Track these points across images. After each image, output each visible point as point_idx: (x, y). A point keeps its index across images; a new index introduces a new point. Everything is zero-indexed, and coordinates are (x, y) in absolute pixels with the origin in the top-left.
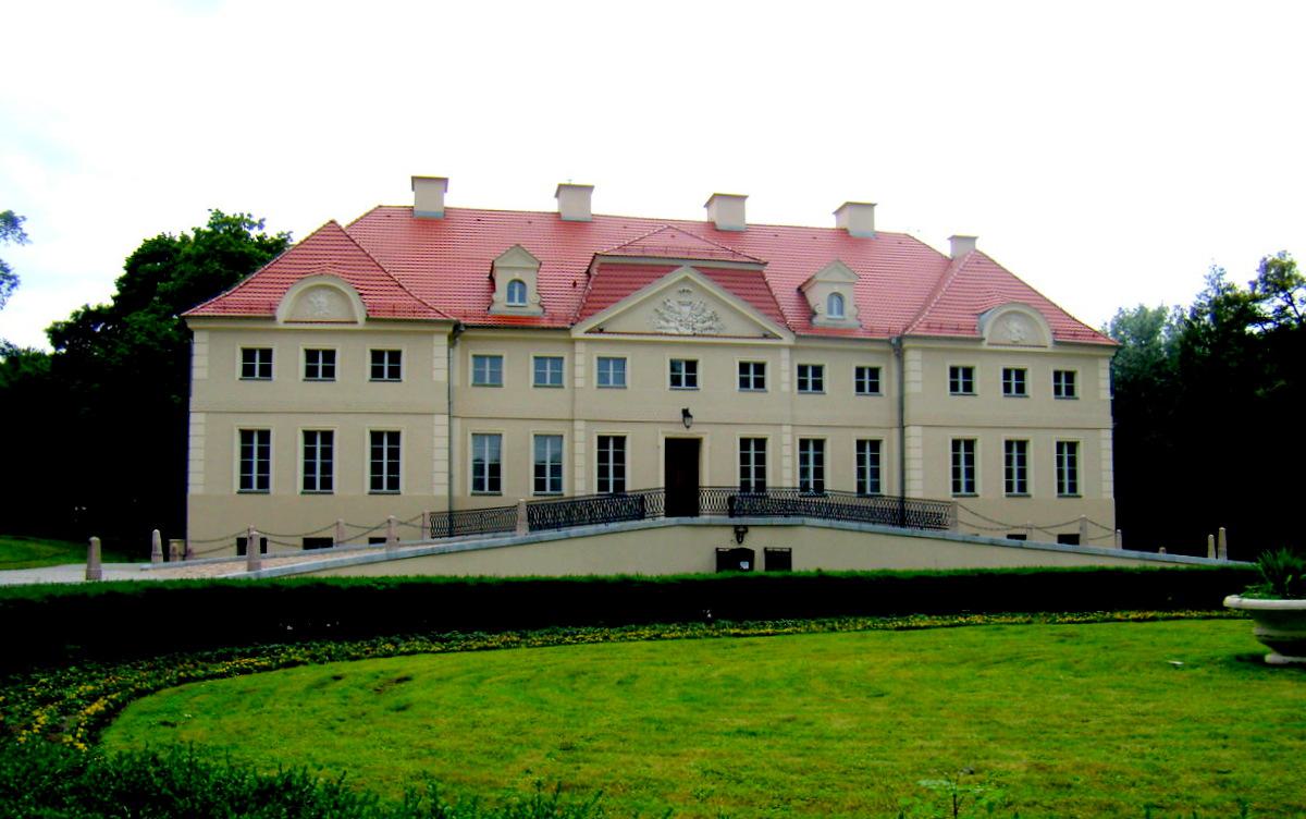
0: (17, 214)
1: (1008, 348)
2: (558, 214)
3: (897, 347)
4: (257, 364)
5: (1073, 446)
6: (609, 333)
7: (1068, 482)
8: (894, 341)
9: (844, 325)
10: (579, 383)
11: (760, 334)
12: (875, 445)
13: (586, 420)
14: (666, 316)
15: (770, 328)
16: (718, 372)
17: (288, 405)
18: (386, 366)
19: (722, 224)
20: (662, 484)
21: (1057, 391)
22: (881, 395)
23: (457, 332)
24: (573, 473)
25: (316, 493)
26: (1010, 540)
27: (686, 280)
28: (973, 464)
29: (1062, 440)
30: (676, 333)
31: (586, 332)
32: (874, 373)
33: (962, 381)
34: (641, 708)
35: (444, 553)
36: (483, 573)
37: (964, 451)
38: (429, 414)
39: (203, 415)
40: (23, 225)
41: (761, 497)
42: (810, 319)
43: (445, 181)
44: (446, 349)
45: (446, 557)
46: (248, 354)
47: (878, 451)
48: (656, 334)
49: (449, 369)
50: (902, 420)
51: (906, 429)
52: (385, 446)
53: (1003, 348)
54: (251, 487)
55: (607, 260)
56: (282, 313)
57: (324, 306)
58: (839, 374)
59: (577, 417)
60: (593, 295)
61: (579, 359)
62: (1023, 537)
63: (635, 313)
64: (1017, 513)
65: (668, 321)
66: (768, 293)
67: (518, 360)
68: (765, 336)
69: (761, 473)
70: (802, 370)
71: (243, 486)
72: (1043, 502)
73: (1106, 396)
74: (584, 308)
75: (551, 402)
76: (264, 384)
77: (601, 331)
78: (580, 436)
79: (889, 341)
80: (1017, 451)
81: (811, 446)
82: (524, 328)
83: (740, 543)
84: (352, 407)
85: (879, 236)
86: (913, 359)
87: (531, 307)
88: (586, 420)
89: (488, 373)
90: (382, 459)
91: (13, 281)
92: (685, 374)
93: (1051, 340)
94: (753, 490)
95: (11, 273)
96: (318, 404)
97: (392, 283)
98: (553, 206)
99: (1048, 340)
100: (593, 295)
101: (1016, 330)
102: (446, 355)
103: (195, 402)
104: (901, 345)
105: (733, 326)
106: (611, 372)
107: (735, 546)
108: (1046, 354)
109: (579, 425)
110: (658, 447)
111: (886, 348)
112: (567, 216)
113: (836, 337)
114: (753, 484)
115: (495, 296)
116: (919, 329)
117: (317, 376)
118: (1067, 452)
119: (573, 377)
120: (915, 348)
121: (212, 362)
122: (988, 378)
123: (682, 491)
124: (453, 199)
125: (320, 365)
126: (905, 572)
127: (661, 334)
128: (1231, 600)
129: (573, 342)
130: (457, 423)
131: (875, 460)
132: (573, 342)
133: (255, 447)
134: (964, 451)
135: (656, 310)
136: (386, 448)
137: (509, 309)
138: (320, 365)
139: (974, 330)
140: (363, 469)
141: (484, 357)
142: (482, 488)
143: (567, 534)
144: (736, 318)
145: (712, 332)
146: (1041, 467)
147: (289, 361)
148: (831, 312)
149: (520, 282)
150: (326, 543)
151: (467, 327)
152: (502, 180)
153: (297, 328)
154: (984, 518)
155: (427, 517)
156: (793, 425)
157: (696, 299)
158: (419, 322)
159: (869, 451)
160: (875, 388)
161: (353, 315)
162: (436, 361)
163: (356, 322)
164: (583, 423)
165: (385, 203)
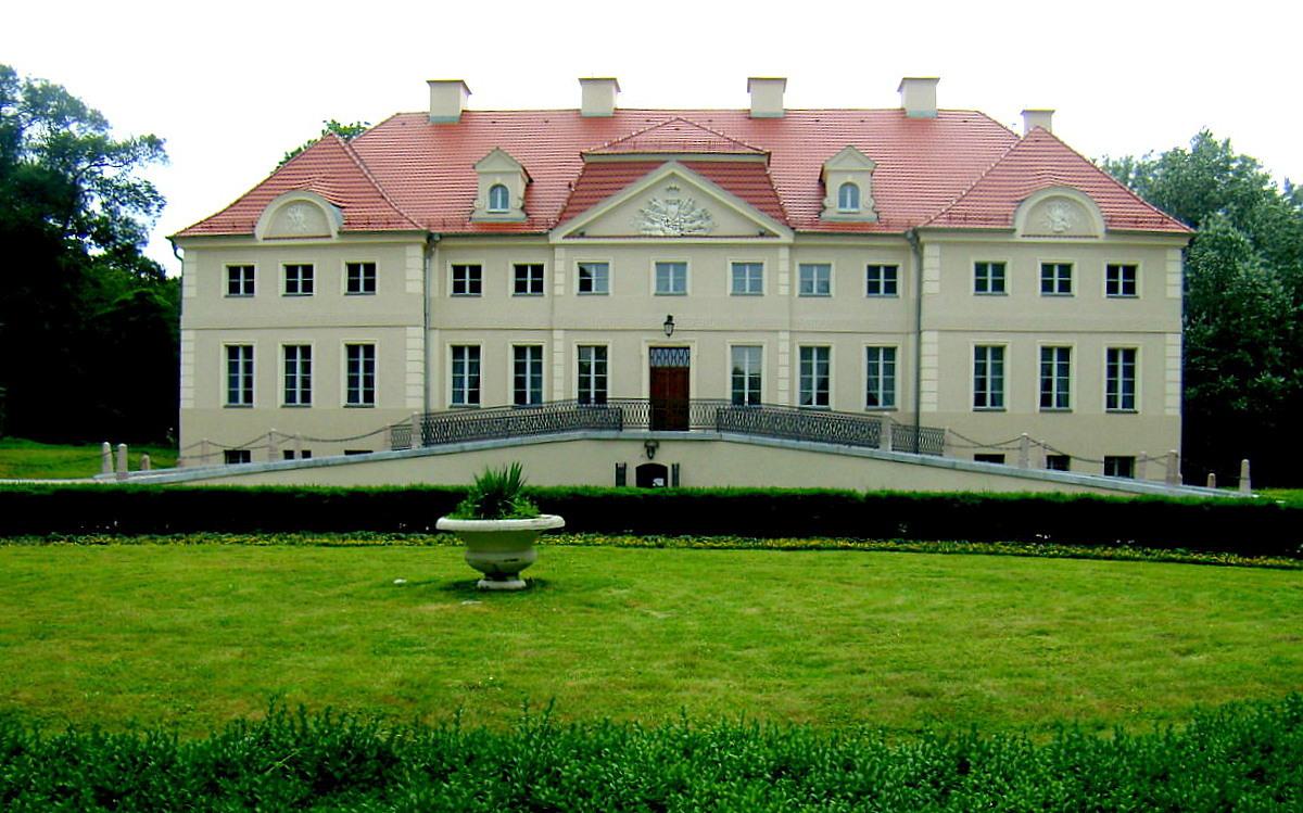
0: (159, 137)
2: (903, 110)
3: (914, 240)
6: (589, 237)
8: (910, 235)
9: (857, 219)
10: (559, 290)
12: (890, 353)
14: (651, 216)
15: (769, 227)
18: (361, 279)
20: (646, 394)
22: (898, 297)
23: (431, 242)
25: (298, 406)
26: (978, 463)
27: (673, 176)
28: (230, 363)
29: (294, 344)
30: (662, 234)
32: (891, 271)
33: (990, 279)
35: (328, 466)
36: (588, 484)
37: (989, 360)
38: (402, 326)
39: (936, 333)
40: (164, 146)
41: (603, 408)
42: (819, 213)
43: (783, 81)
44: (421, 262)
45: (332, 469)
46: (521, 271)
47: (1002, 359)
48: (640, 236)
49: (425, 282)
51: (923, 334)
52: (815, 361)
56: (261, 231)
59: (555, 327)
60: (577, 197)
61: (560, 266)
62: (999, 459)
64: (1057, 432)
65: (653, 222)
68: (762, 235)
71: (1043, 404)
73: (1176, 292)
74: (565, 211)
75: (749, 311)
77: (582, 235)
78: (559, 346)
79: (904, 236)
80: (297, 357)
81: (528, 352)
82: (506, 235)
83: (651, 458)
84: (329, 320)
85: (940, 115)
86: (932, 255)
88: (940, 331)
91: (160, 202)
92: (672, 277)
94: (593, 401)
95: (159, 195)
98: (895, 101)
99: (1099, 228)
100: (577, 197)
102: (421, 266)
104: (918, 239)
105: (725, 225)
107: (645, 461)
108: (332, 246)
109: (558, 335)
110: (641, 357)
112: (912, 111)
114: (593, 396)
115: (826, 202)
117: (296, 291)
118: (1122, 363)
119: (553, 285)
120: (933, 243)
122: (1023, 275)
124: (792, 100)
125: (299, 280)
127: (645, 236)
128: (444, 522)
129: (553, 247)
130: (435, 336)
131: (890, 370)
134: (989, 360)
135: (642, 211)
136: (361, 358)
137: (492, 215)
138: (299, 280)
139: (1007, 220)
140: (338, 382)
141: (668, 264)
143: (462, 447)
144: (730, 214)
146: (1088, 379)
147: (271, 278)
148: (493, 205)
149: (502, 186)
151: (441, 236)
153: (275, 244)
154: (968, 440)
156: (791, 332)
158: (392, 234)
159: (881, 359)
160: (891, 288)
161: (330, 231)
162: (409, 276)
163: (330, 236)
165: (403, 110)
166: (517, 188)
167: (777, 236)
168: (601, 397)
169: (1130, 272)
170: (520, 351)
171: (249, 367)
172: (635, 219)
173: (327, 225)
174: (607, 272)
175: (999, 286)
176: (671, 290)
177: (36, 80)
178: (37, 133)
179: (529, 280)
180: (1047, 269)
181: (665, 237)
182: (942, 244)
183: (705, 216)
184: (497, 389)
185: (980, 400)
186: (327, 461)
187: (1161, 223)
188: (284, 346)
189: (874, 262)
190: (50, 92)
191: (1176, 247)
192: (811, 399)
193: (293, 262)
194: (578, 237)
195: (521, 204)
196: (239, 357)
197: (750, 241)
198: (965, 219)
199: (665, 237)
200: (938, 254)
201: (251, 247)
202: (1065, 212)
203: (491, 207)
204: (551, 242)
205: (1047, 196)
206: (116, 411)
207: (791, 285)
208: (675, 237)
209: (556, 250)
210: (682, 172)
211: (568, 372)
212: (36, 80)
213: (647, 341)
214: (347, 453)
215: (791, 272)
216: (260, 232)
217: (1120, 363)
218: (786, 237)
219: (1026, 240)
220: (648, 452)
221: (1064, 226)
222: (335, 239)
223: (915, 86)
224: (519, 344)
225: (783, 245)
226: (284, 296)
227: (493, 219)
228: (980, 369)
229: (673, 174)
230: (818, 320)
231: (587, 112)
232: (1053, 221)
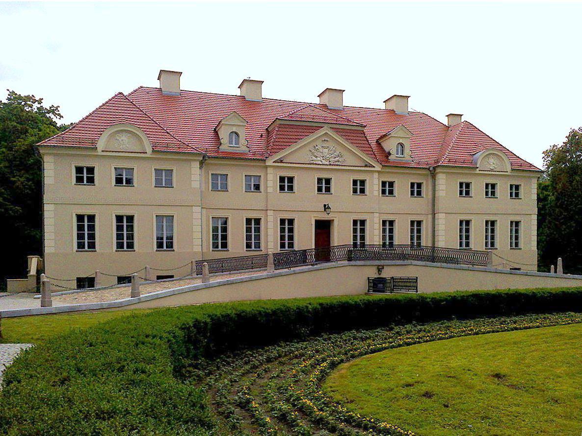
5: (391, 223)
7: (515, 243)
8: (431, 169)
9: (238, 150)
10: (270, 190)
11: (364, 165)
12: (419, 223)
16: (342, 185)
18: (164, 179)
19: (331, 105)
21: (412, 193)
27: (326, 133)
31: (273, 162)
33: (465, 189)
37: (466, 224)
39: (444, 214)
42: (387, 157)
50: (433, 210)
55: (283, 122)
56: (101, 145)
57: (125, 143)
58: (402, 186)
61: (270, 177)
63: (301, 152)
65: (316, 157)
66: (367, 142)
67: (237, 178)
68: (366, 166)
69: (363, 238)
70: (282, 179)
77: (281, 162)
78: (270, 219)
79: (429, 169)
86: (441, 178)
87: (243, 148)
89: (220, 184)
90: (222, 235)
92: (324, 186)
96: (125, 200)
97: (162, 131)
99: (509, 168)
101: (492, 163)
103: (46, 198)
105: (350, 160)
106: (219, 182)
107: (377, 276)
109: (270, 213)
111: (428, 172)
113: (402, 167)
116: (443, 161)
120: (50, 154)
123: (324, 250)
124: (186, 84)
129: (266, 167)
132: (266, 167)
133: (86, 226)
134: (466, 224)
138: (491, 190)
142: (217, 247)
144: (353, 156)
148: (231, 142)
149: (236, 133)
152: (211, 76)
153: (109, 155)
155: (194, 264)
156: (379, 213)
157: (331, 144)
158: (182, 153)
160: (419, 193)
164: (378, 214)
167: (374, 167)
169: (391, 184)
170: (80, 218)
173: (143, 146)
175: (91, 180)
176: (219, 189)
182: (55, 155)
183: (340, 156)
184: (237, 244)
187: (449, 161)
189: (413, 181)
191: (534, 177)
192: (218, 245)
197: (359, 168)
198: (521, 166)
200: (53, 161)
203: (229, 144)
204: (267, 164)
209: (268, 169)
210: (330, 132)
211: (275, 232)
213: (314, 217)
217: (359, 227)
219: (481, 172)
221: (494, 167)
223: (332, 93)
224: (118, 214)
226: (75, 184)
227: (230, 150)
228: (119, 228)
230: (389, 207)
232: (490, 164)
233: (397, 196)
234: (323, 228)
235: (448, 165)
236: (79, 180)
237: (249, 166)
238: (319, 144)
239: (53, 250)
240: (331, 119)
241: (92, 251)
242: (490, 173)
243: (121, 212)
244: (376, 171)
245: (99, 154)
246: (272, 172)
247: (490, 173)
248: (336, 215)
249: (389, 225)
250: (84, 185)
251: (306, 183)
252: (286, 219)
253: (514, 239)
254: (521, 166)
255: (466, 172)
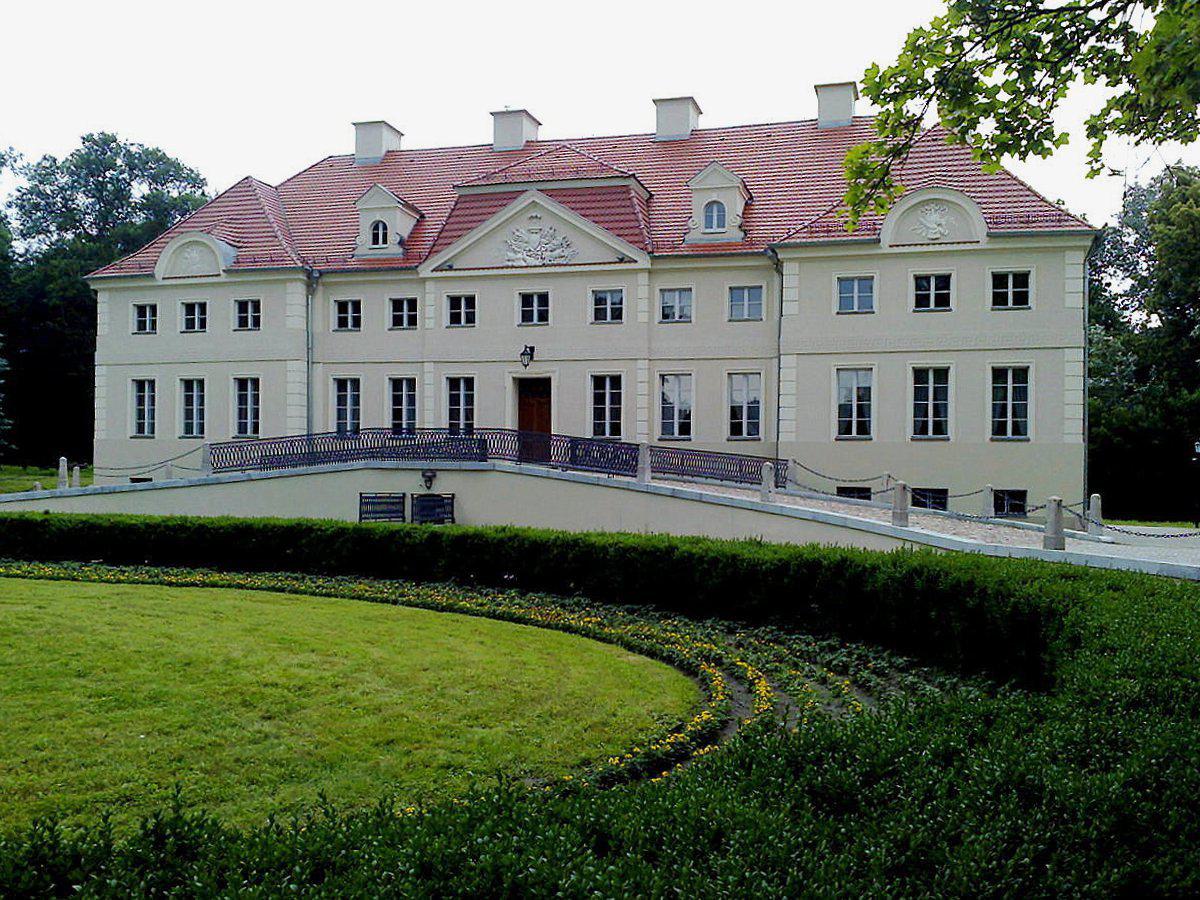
1: (925, 249)
4: (146, 319)
6: (456, 270)
10: (430, 324)
13: (434, 362)
16: (571, 304)
17: (169, 355)
18: (248, 315)
23: (313, 280)
24: (308, 410)
27: (533, 202)
30: (524, 264)
34: (36, 626)
52: (931, 385)
53: (919, 249)
54: (1005, 433)
61: (430, 299)
65: (515, 252)
68: (621, 261)
71: (995, 432)
72: (970, 455)
76: (1020, 314)
77: (451, 268)
78: (429, 378)
83: (429, 488)
92: (534, 308)
93: (986, 230)
99: (980, 230)
105: (586, 252)
118: (1010, 387)
120: (104, 290)
121: (113, 316)
123: (533, 436)
125: (195, 316)
126: (219, 519)
127: (507, 267)
129: (424, 280)
130: (318, 369)
137: (706, 236)
138: (195, 316)
142: (1004, 433)
144: (591, 242)
145: (561, 261)
146: (970, 403)
147: (171, 316)
148: (709, 225)
150: (864, 493)
151: (321, 273)
153: (176, 282)
158: (272, 269)
163: (219, 275)
166: (735, 206)
168: (469, 428)
171: (470, 400)
172: (500, 250)
174: (759, 297)
175: (1021, 299)
177: (132, 144)
178: (139, 190)
179: (404, 313)
180: (921, 281)
181: (526, 267)
182: (801, 260)
185: (999, 429)
186: (115, 488)
188: (181, 380)
190: (157, 157)
193: (528, 290)
194: (446, 270)
195: (739, 221)
196: (144, 387)
199: (526, 267)
201: (154, 286)
202: (942, 217)
204: (421, 276)
205: (920, 199)
206: (14, 447)
207: (651, 312)
208: (535, 266)
209: (427, 283)
210: (542, 200)
212: (132, 144)
214: (134, 480)
215: (650, 299)
216: (887, 237)
218: (644, 262)
220: (426, 481)
222: (984, 244)
225: (642, 270)
228: (920, 394)
229: (533, 202)
231: (664, 135)
233: (1034, 308)
234: (534, 394)
235: (810, 240)
236: (999, 300)
237: (128, 288)
238: (522, 228)
239: (792, 438)
240: (500, 179)
241: (866, 439)
242: (931, 248)
243: (923, 362)
244: (642, 269)
245: (886, 252)
246: (433, 290)
247: (931, 248)
248: (555, 367)
249: (403, 389)
250: (932, 311)
251: (499, 306)
252: (403, 379)
253: (195, 411)
254: (1027, 222)
255: (669, 266)
